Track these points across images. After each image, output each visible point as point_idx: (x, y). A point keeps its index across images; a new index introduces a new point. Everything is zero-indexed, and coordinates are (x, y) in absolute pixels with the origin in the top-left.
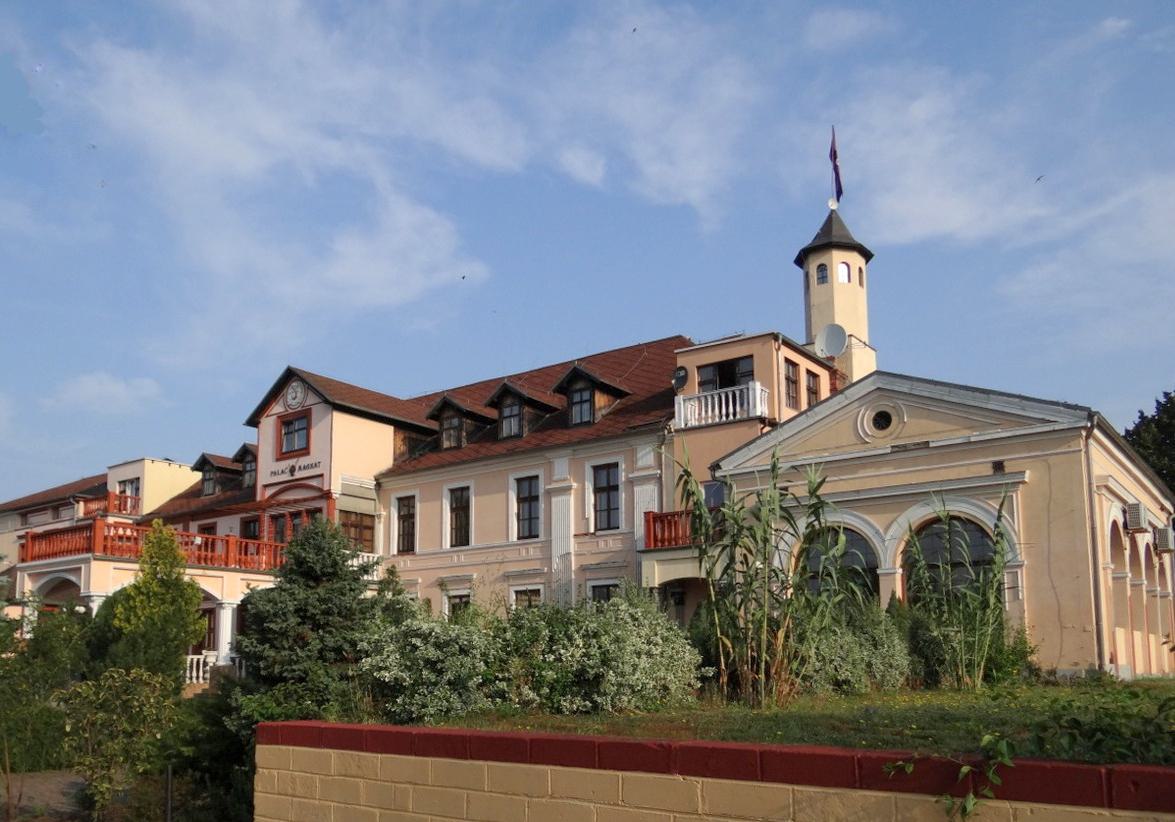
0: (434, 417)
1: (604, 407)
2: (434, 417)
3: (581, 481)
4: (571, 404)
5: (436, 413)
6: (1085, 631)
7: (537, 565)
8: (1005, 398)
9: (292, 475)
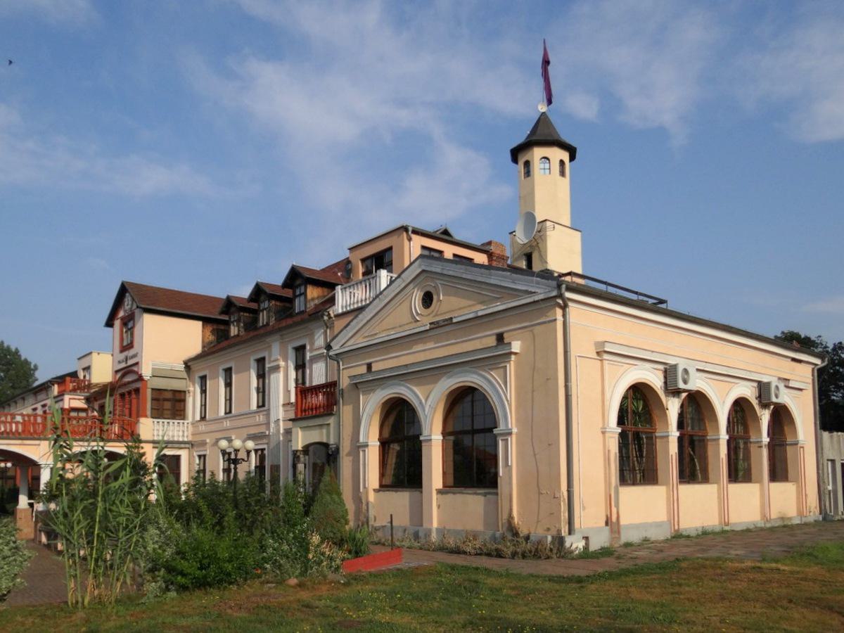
0: (223, 313)
1: (318, 298)
2: (223, 313)
3: (286, 360)
4: (295, 296)
5: (224, 309)
6: (555, 498)
7: (262, 429)
8: (500, 272)
9: (126, 363)
